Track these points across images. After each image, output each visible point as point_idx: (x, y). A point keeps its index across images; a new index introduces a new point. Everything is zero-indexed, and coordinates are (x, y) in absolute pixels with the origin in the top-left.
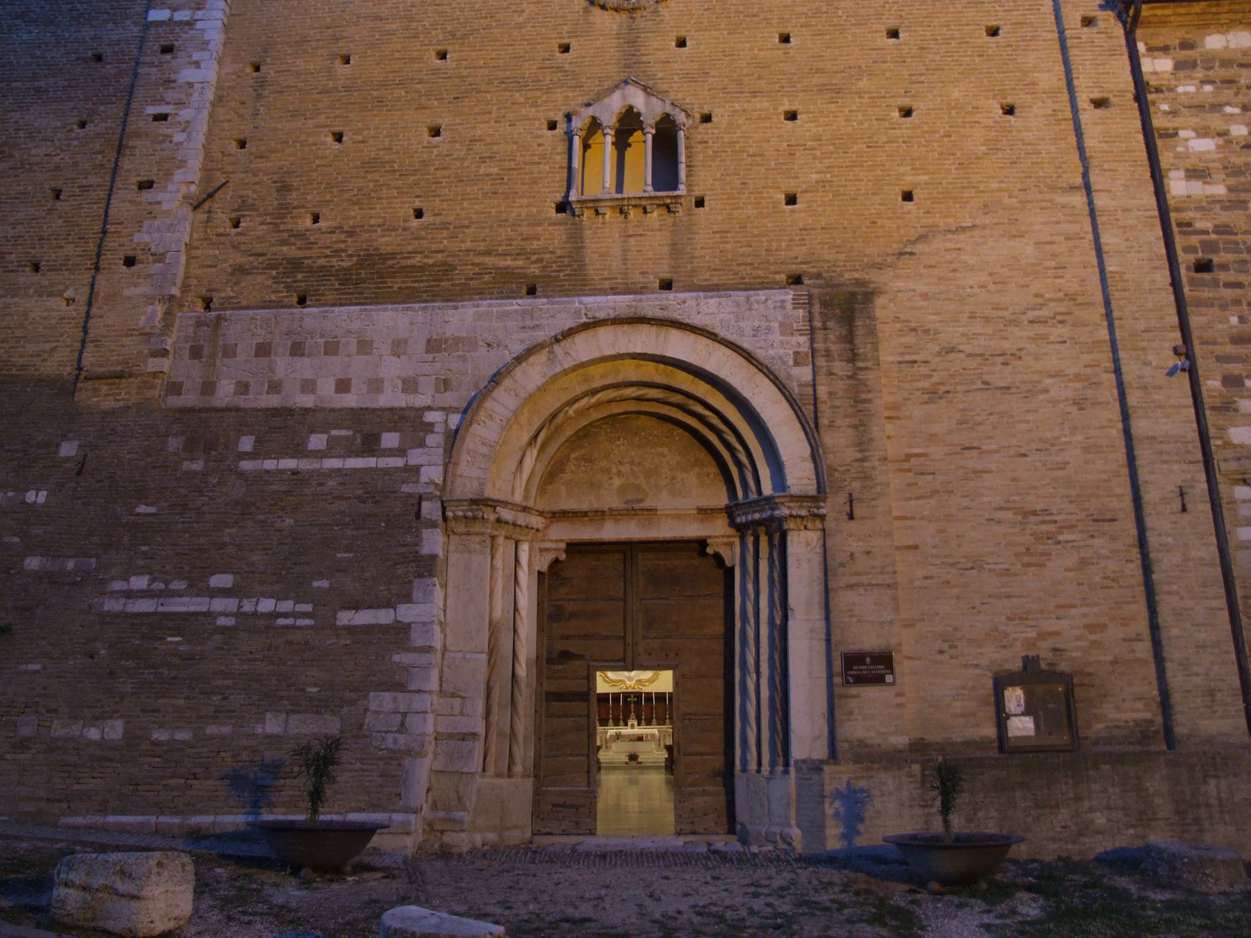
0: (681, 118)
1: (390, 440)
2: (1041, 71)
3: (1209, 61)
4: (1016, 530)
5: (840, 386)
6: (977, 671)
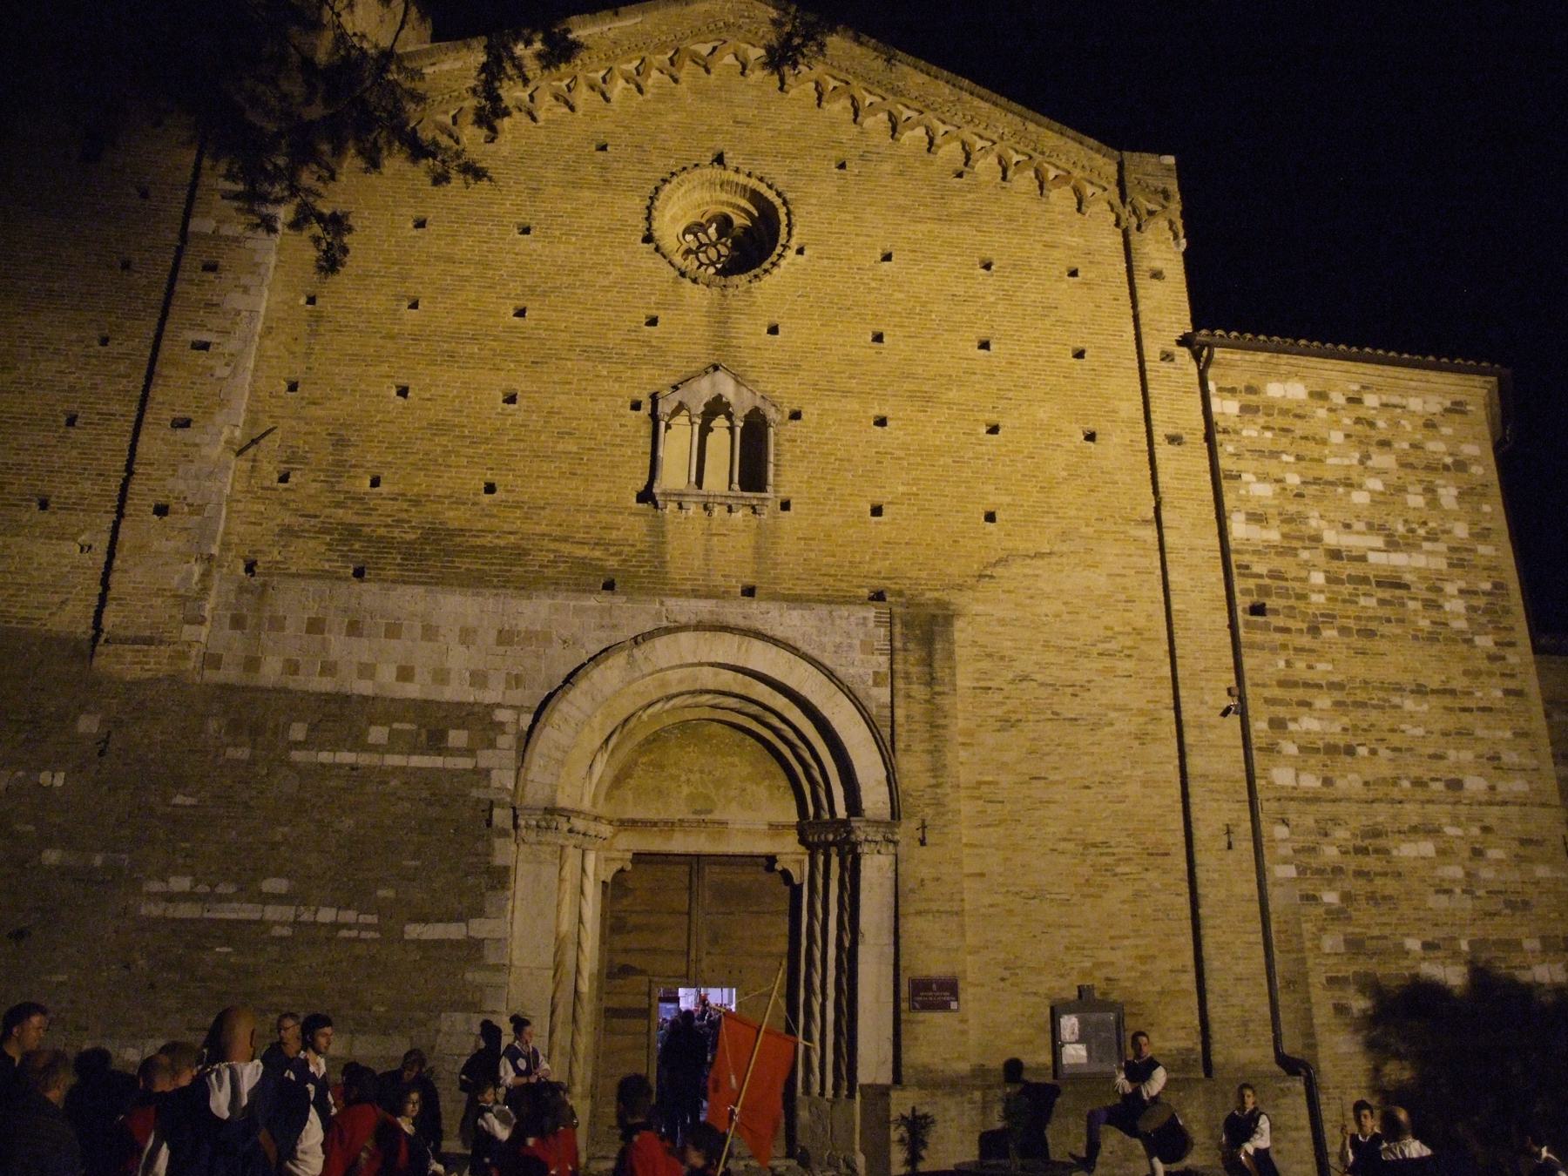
0: (771, 414)
1: (457, 738)
2: (1121, 400)
3: (1269, 408)
4: (1076, 861)
5: (917, 710)
6: (1037, 999)
